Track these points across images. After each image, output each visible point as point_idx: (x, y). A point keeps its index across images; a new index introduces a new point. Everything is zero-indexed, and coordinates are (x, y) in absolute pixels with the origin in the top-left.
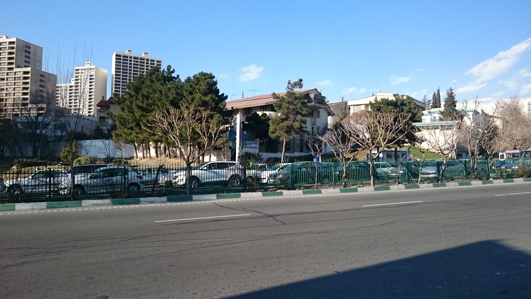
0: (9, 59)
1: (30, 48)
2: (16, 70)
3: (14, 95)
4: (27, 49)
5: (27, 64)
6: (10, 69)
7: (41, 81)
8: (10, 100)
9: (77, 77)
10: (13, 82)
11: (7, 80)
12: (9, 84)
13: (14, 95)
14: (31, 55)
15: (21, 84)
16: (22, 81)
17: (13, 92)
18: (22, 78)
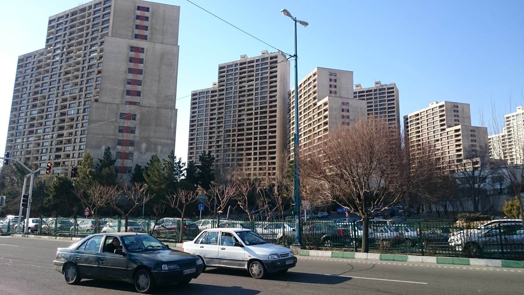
1: (457, 107)
4: (455, 109)
7: (471, 135)
12: (444, 144)
14: (460, 114)
15: (454, 142)
18: (454, 136)
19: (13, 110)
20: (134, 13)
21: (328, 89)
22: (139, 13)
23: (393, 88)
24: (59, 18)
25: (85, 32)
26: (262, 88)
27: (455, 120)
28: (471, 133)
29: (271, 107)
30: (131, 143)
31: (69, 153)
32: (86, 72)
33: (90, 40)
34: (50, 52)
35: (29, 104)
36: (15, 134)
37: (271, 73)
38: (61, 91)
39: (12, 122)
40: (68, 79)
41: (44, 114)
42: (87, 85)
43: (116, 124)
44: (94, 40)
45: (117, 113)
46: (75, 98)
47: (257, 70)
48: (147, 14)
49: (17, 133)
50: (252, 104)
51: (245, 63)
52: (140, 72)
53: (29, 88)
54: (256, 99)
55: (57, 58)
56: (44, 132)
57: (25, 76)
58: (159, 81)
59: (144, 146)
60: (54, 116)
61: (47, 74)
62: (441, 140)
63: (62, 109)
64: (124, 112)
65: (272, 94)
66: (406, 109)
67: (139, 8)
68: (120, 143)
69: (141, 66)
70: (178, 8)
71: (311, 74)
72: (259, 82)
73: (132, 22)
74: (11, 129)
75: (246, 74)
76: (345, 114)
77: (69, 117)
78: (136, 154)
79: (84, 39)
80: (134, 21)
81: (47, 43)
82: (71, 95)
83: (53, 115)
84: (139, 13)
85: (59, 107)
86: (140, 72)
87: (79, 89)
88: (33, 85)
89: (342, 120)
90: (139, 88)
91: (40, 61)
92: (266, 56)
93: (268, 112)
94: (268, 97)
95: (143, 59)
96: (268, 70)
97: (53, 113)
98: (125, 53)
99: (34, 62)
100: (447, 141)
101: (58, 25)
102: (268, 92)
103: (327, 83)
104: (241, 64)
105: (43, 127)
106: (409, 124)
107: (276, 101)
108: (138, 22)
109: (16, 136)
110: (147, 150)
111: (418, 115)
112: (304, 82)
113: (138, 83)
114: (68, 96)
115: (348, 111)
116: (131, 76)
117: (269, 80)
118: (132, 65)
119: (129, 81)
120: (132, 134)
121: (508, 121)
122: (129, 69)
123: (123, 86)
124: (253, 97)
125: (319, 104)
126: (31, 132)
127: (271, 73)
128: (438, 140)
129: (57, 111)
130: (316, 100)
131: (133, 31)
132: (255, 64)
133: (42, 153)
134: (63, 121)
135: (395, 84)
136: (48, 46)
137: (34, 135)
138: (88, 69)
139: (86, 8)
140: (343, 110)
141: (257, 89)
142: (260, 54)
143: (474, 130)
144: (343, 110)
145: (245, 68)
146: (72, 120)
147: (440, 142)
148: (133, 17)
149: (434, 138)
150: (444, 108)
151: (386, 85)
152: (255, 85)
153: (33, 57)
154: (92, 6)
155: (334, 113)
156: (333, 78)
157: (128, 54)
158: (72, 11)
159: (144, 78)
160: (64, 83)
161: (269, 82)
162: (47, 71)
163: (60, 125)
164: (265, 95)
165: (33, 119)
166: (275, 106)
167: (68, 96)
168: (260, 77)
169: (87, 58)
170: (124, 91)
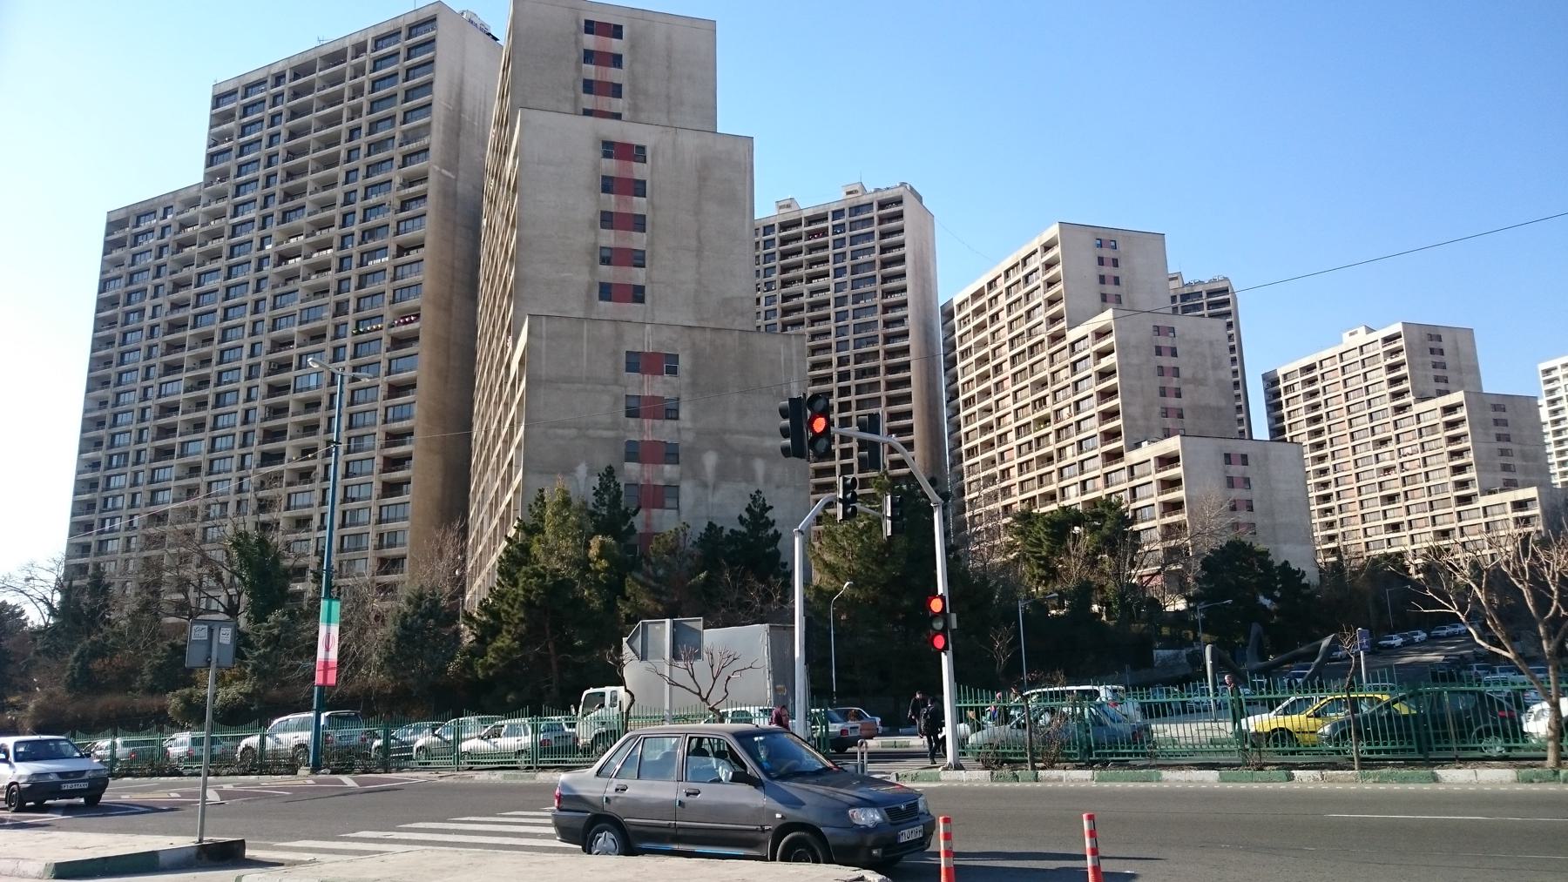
0: (1393, 382)
1: (1439, 338)
2: (1418, 408)
3: (1427, 479)
4: (1434, 344)
5: (1442, 386)
6: (1399, 409)
7: (1496, 422)
8: (1417, 493)
9: (1551, 392)
10: (1418, 441)
11: (1398, 441)
12: (1409, 450)
13: (1427, 479)
14: (1447, 358)
15: (1443, 442)
16: (1443, 434)
17: (1423, 470)
18: (1441, 427)
19: (96, 382)
20: (577, 42)
21: (1094, 289)
22: (590, 42)
23: (1226, 291)
24: (249, 88)
25: (345, 126)
26: (857, 298)
27: (1437, 379)
28: (1493, 415)
29: (890, 354)
30: (670, 454)
31: (306, 511)
32: (354, 250)
33: (364, 149)
34: (221, 196)
35: (151, 362)
36: (104, 462)
37: (884, 250)
38: (267, 314)
39: (91, 423)
40: (291, 277)
41: (210, 392)
42: (363, 291)
43: (616, 389)
44: (378, 151)
45: (615, 353)
46: (318, 336)
47: (839, 243)
48: (615, 46)
49: (111, 457)
50: (828, 347)
51: (797, 223)
52: (639, 223)
53: (149, 312)
54: (841, 331)
55: (252, 213)
56: (212, 450)
57: (131, 275)
58: (699, 252)
59: (710, 460)
60: (245, 399)
61: (215, 265)
62: (1398, 441)
63: (271, 372)
64: (639, 349)
65: (891, 315)
66: (1269, 347)
67: (590, 27)
68: (634, 452)
69: (639, 205)
70: (708, 29)
71: (1037, 244)
72: (847, 277)
73: (572, 72)
74: (88, 444)
75: (802, 257)
76: (1167, 361)
77: (301, 395)
78: (687, 488)
79: (342, 148)
80: (579, 69)
81: (208, 166)
82: (305, 327)
83: (243, 395)
84: (590, 42)
85: (263, 368)
86: (639, 223)
87: (332, 306)
88: (164, 300)
89: (1158, 382)
90: (638, 276)
91: (183, 226)
92: (865, 200)
93: (882, 370)
94: (881, 323)
95: (644, 182)
96: (876, 242)
97: (243, 385)
98: (587, 163)
99: (164, 229)
100: (1418, 441)
101: (246, 110)
102: (880, 308)
103: (1091, 270)
104: (784, 226)
105: (206, 435)
106: (1283, 398)
107: (905, 335)
108: (591, 72)
109: (109, 467)
110: (723, 473)
111: (1310, 368)
112: (1007, 272)
113: (637, 259)
114: (295, 329)
115: (1174, 353)
116: (609, 238)
117: (878, 272)
118: (611, 202)
119: (606, 253)
120: (669, 423)
121: (1549, 381)
122: (603, 213)
123: (586, 269)
124: (831, 325)
125: (1072, 335)
126: (165, 453)
127: (884, 250)
128: (1383, 442)
129: (258, 381)
130: (1064, 324)
131: (576, 100)
132: (829, 224)
133: (207, 517)
134: (278, 411)
135: (1226, 279)
136: (210, 178)
137: (175, 462)
138: (363, 240)
139: (344, 51)
140: (1159, 351)
141: (840, 301)
142: (843, 195)
143: (1500, 404)
144: (1159, 351)
145: (798, 238)
146: (312, 405)
147: (1392, 446)
148: (575, 55)
149: (1373, 433)
150: (1401, 343)
151: (1201, 282)
152: (832, 287)
153: (160, 213)
154: (365, 43)
155: (1135, 360)
156: (1107, 253)
157: (597, 167)
158: (295, 63)
159: (651, 243)
160: (278, 291)
161: (879, 278)
162: (215, 255)
163: (158, 443)
164: (870, 318)
165: (170, 409)
166: (906, 350)
167: (295, 329)
168: (848, 262)
169: (358, 206)
170: (590, 286)
